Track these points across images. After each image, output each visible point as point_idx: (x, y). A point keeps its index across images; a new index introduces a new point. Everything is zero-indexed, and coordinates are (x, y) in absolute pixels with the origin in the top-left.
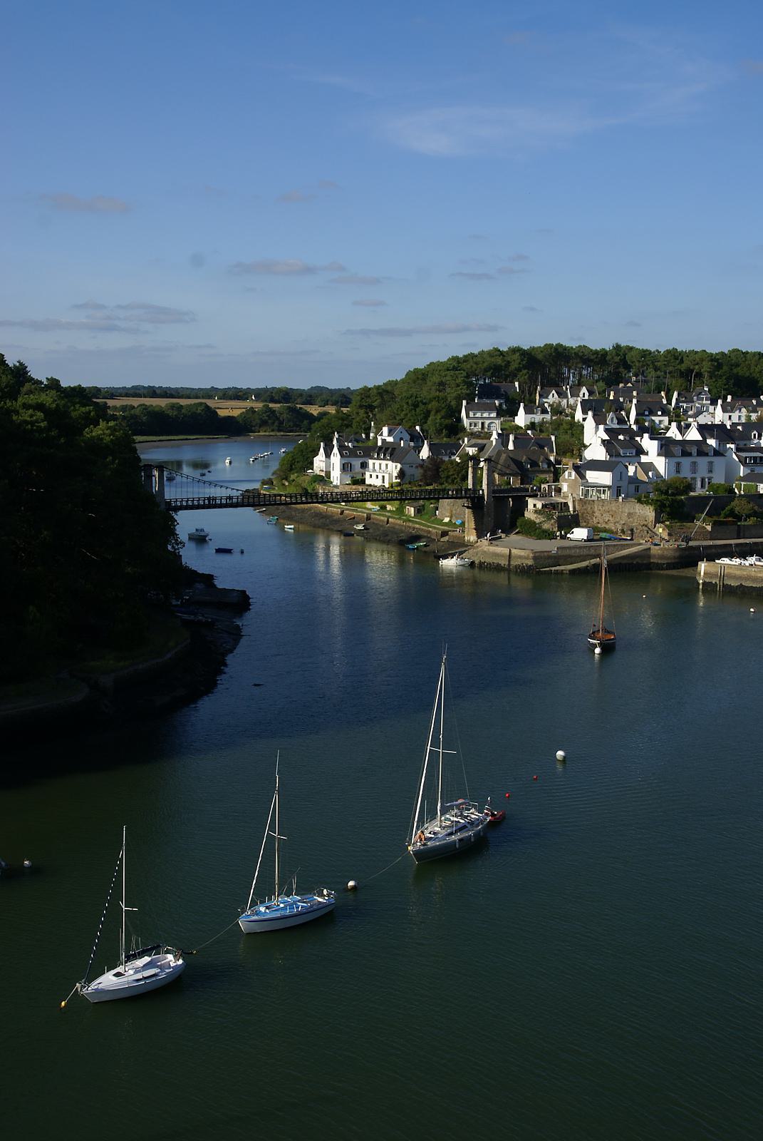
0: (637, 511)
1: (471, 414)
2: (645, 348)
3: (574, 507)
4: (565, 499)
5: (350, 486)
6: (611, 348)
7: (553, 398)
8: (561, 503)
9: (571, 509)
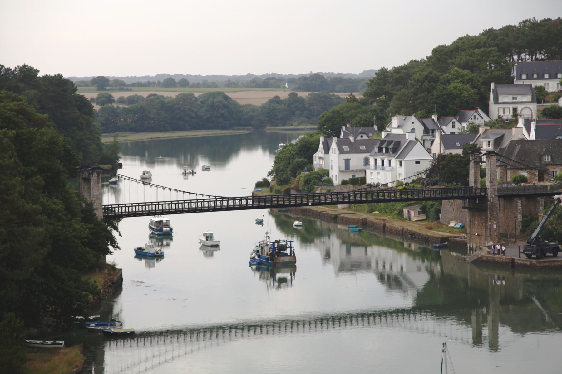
1: (501, 99)
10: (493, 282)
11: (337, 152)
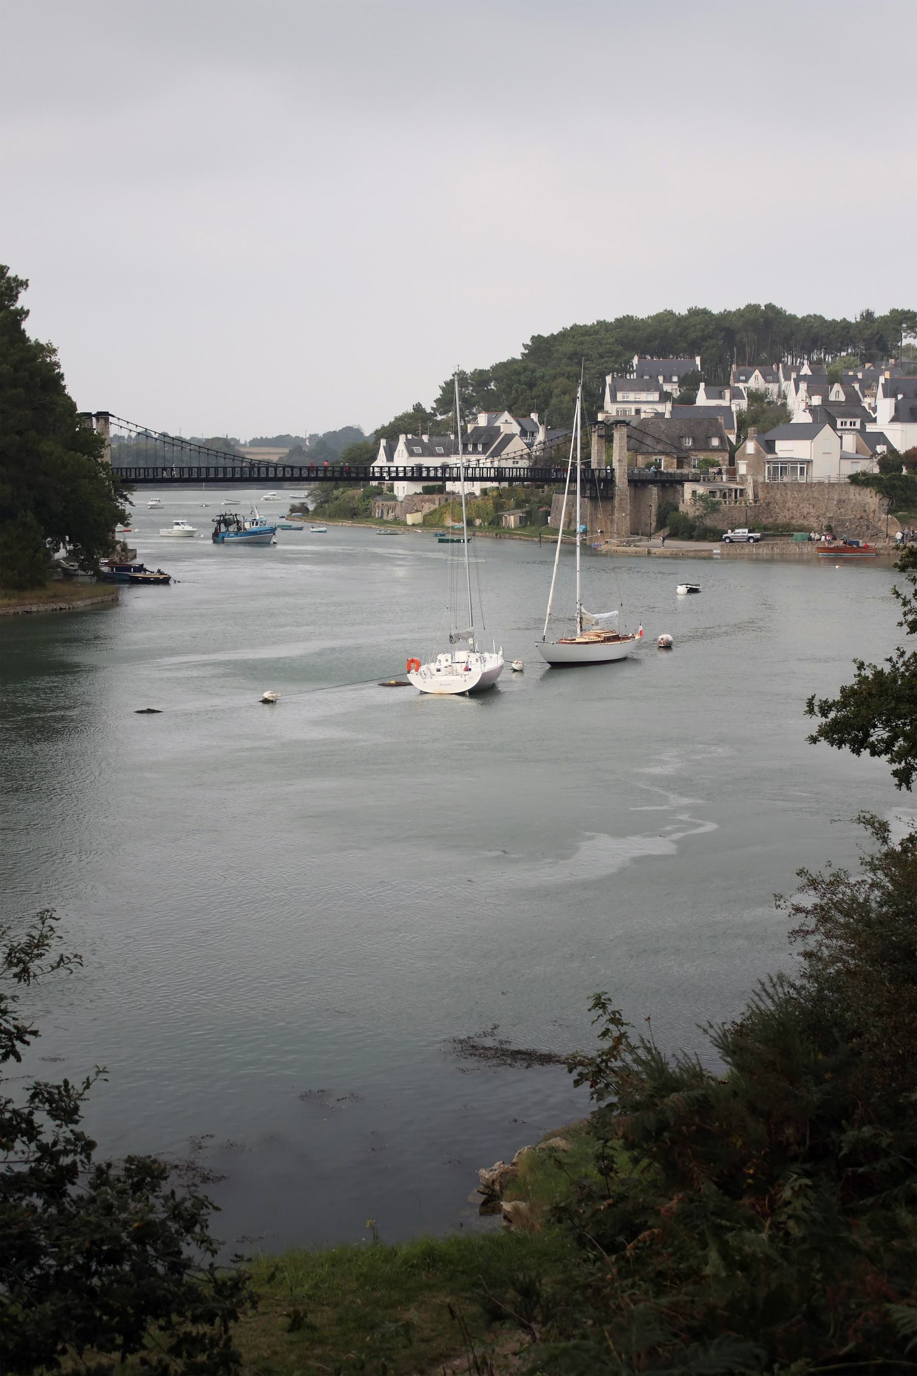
0: (852, 496)
1: (620, 396)
2: (906, 309)
3: (756, 495)
4: (742, 484)
5: (421, 496)
6: (858, 319)
7: (756, 381)
8: (736, 490)
9: (751, 497)
10: (724, 1222)
11: (406, 454)
